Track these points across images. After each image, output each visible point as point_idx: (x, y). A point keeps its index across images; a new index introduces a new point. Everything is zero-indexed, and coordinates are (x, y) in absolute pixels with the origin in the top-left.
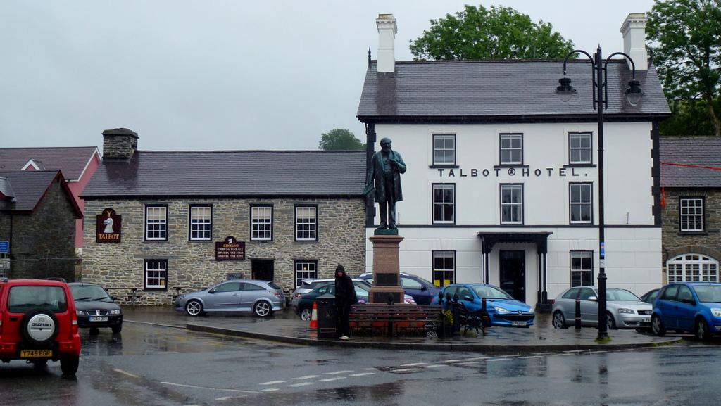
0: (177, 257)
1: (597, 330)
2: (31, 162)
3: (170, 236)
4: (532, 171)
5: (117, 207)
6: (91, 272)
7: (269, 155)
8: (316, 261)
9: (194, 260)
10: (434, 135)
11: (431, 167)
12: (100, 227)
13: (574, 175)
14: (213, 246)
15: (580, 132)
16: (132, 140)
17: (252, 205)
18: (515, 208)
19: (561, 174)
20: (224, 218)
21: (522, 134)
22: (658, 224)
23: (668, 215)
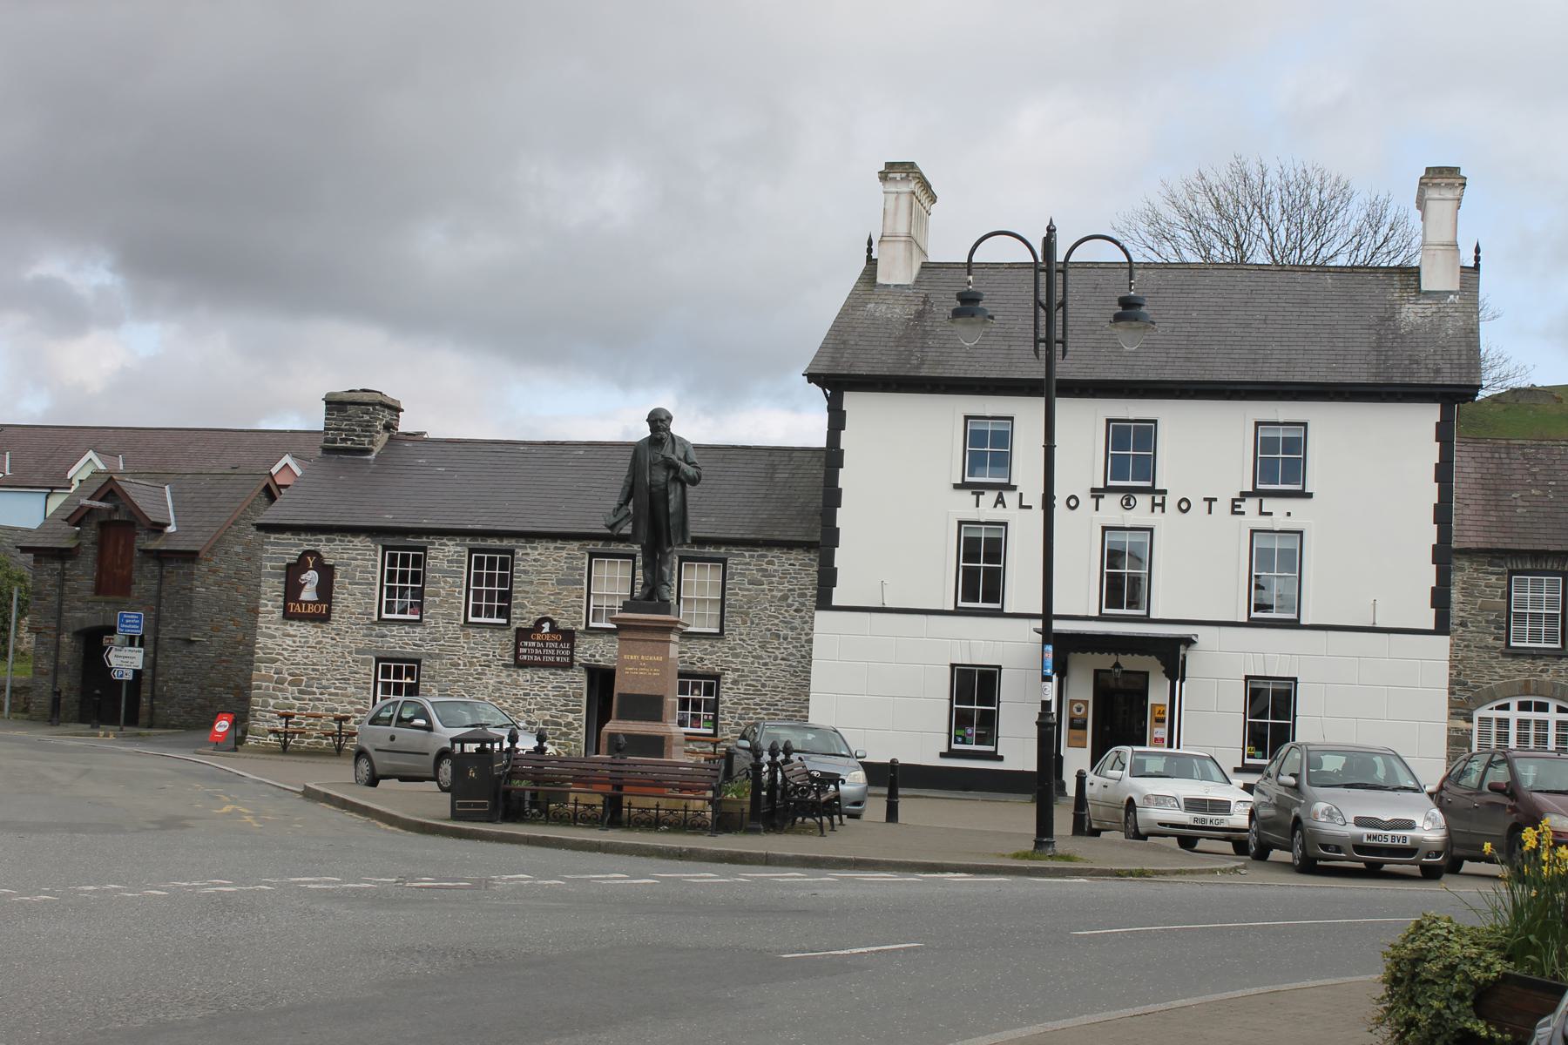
0: (439, 657)
1: (448, 796)
2: (287, 459)
3: (429, 611)
4: (1171, 502)
5: (330, 549)
6: (270, 679)
7: (497, 448)
8: (717, 677)
9: (472, 664)
10: (967, 418)
11: (956, 486)
12: (292, 589)
13: (1261, 513)
14: (511, 633)
15: (988, 414)
16: (386, 416)
17: (592, 555)
18: (1135, 581)
19: (1235, 510)
20: (534, 578)
21: (1305, 424)
22: (1442, 627)
23: (1481, 609)
